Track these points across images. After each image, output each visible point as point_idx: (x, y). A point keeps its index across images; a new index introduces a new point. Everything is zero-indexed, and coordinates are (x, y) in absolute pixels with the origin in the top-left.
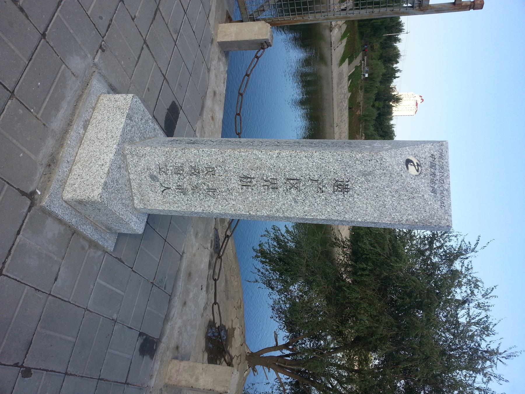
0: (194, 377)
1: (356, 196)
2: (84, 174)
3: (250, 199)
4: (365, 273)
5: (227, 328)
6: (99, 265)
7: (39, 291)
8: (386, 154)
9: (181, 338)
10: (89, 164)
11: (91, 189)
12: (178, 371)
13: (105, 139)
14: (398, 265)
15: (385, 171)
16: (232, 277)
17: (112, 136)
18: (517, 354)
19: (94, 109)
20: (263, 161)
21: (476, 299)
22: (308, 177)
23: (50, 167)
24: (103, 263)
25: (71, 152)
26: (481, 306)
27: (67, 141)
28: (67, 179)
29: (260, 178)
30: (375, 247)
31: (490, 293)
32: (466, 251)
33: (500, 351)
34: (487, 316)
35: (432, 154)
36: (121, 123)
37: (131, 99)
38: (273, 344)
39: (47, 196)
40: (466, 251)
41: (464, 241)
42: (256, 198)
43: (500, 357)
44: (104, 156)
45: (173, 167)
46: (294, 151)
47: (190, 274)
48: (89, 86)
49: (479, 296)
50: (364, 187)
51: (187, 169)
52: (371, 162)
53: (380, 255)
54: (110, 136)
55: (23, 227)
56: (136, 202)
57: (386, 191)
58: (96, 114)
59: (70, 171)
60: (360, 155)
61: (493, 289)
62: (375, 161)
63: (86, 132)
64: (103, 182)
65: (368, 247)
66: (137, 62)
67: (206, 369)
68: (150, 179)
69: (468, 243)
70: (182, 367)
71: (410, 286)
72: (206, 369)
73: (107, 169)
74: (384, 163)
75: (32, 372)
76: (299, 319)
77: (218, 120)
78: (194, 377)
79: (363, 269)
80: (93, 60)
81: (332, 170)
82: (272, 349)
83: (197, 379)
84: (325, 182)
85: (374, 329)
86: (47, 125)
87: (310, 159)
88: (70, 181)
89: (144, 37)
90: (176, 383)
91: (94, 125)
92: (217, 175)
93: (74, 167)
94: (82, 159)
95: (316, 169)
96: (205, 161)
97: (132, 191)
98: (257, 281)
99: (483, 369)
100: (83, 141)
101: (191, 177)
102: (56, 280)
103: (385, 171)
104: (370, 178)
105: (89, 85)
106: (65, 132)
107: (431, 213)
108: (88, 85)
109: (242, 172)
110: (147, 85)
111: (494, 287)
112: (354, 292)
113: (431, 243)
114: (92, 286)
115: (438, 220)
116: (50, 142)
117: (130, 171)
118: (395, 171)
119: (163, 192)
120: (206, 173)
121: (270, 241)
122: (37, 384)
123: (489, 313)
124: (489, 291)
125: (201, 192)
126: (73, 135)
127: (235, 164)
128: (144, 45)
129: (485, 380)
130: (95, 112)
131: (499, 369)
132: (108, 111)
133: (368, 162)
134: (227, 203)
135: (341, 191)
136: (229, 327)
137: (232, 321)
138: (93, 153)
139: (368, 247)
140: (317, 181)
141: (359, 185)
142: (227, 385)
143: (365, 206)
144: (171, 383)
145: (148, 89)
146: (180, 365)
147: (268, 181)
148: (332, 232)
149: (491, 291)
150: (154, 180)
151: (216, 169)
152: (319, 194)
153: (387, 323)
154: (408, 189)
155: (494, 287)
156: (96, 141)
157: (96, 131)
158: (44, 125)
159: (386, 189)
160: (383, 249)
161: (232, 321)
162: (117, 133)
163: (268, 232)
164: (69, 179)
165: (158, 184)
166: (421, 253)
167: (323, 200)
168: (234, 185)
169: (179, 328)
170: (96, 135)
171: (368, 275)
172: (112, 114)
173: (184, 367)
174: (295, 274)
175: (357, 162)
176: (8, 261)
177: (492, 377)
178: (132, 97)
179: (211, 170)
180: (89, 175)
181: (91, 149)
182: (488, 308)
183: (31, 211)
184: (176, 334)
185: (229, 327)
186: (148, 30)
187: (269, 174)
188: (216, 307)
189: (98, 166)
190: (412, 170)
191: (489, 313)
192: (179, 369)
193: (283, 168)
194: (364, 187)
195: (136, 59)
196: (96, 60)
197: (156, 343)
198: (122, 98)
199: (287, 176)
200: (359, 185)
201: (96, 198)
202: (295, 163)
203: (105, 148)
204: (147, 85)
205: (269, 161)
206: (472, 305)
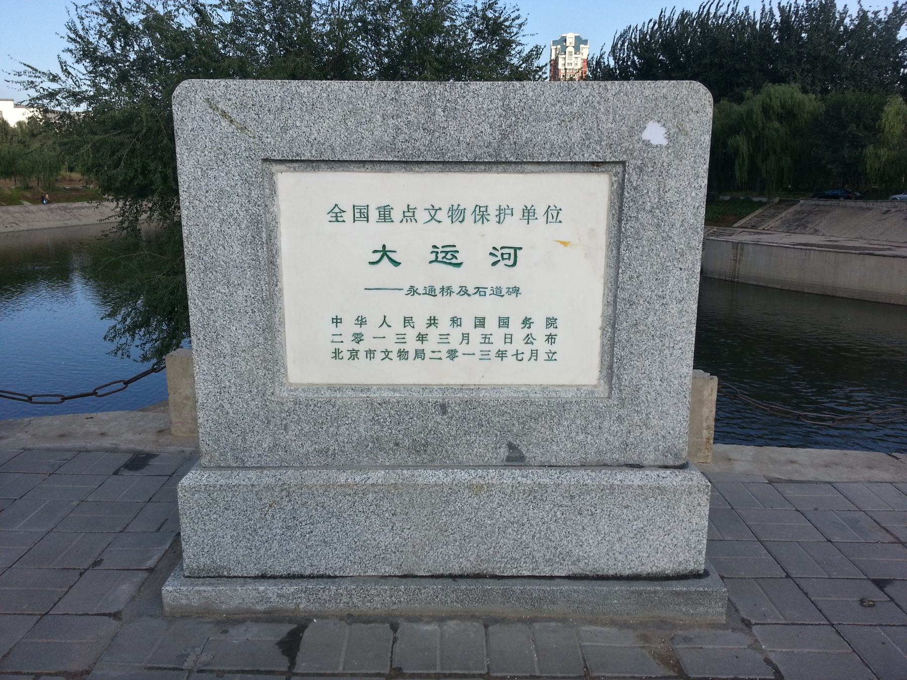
0: (185, 402)
4: (172, 174)
14: (144, 120)
30: (120, 159)
41: (87, 6)
47: (62, 436)
78: (185, 402)
113: (104, 60)
121: (137, 342)
146: (176, 423)
148: (112, 235)
160: (122, 144)
163: (118, 349)
166: (123, 77)
188: (100, 392)
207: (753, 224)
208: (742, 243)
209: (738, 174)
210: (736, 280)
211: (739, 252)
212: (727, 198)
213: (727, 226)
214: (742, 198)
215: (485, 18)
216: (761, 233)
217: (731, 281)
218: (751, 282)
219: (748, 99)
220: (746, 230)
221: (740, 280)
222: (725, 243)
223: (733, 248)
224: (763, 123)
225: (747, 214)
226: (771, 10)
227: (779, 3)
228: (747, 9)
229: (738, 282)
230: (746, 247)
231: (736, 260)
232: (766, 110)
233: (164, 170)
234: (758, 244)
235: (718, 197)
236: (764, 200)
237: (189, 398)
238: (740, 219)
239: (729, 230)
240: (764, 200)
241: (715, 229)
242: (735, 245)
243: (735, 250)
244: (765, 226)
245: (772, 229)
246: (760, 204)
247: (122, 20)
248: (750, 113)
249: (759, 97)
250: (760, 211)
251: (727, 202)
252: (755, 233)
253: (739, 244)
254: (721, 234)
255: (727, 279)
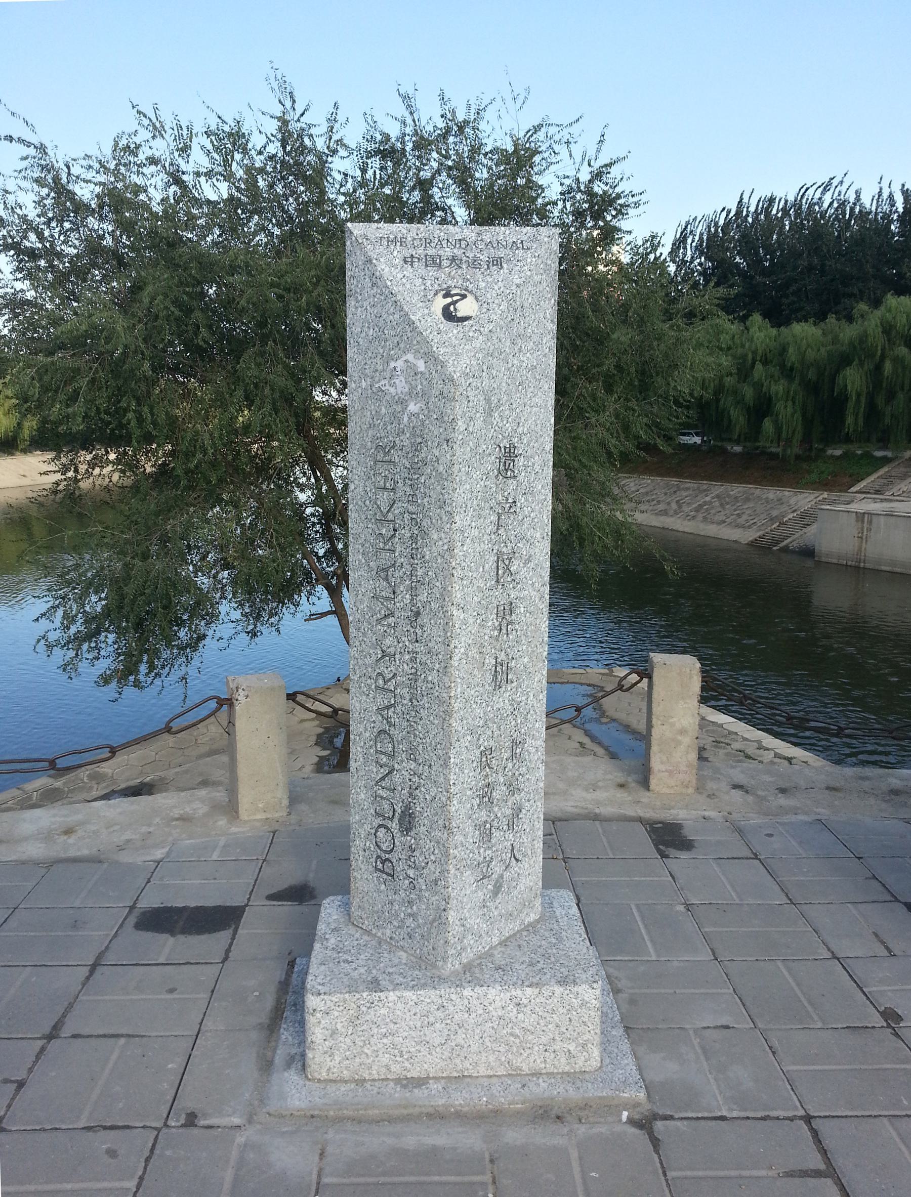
0: (679, 738)
1: (520, 430)
2: (544, 1040)
3: (526, 660)
5: (321, 730)
6: (630, 964)
7: (771, 1048)
8: (453, 365)
9: (600, 784)
10: (517, 1036)
11: (579, 1011)
12: (670, 773)
13: (448, 1021)
15: (485, 368)
16: (199, 741)
17: (438, 1009)
18: (279, 77)
19: (361, 1082)
20: (470, 642)
21: (168, 154)
22: (493, 536)
23: (560, 1115)
24: (619, 958)
25: (499, 1089)
26: (182, 144)
27: (481, 1105)
28: (558, 1073)
29: (495, 643)
31: (150, 120)
32: (45, 168)
33: (278, 111)
34: (208, 134)
35: (402, 262)
36: (402, 999)
37: (326, 997)
38: (333, 620)
39: (625, 1095)
40: (45, 168)
42: (524, 647)
43: (291, 116)
44: (495, 1009)
45: (479, 847)
46: (454, 572)
48: (316, 1113)
49: (159, 143)
50: (507, 412)
51: (483, 815)
52: (471, 398)
53: (93, 380)
54: (440, 1014)
55: (706, 1115)
56: (533, 917)
57: (513, 366)
58: (374, 1072)
59: (537, 1074)
60: (460, 423)
61: (139, 112)
62: (469, 389)
63: (428, 1078)
64: (562, 989)
65: (78, 408)
66: (129, 1036)
67: (661, 718)
68: (500, 895)
69: (25, 164)
70: (663, 768)
71: (166, 308)
72: (661, 718)
73: (529, 991)
74: (473, 370)
75: (883, 1008)
76: (278, 566)
77: (58, 819)
78: (679, 738)
79: (140, 420)
80: (243, 1128)
81: (482, 483)
82: (343, 622)
83: (683, 732)
84: (500, 498)
85: (277, 395)
86: (487, 1156)
87: (466, 535)
88: (563, 1065)
89: (40, 1043)
90: (694, 771)
91: (407, 1064)
92: (492, 743)
93: (526, 1069)
94: (503, 1059)
95: (482, 520)
96: (471, 775)
97: (518, 931)
98: (184, 678)
99: (319, 156)
100: (455, 1074)
101: (495, 801)
102: (727, 1027)
103: (485, 368)
104: (494, 399)
105: (312, 1112)
106: (461, 1117)
107: (542, 271)
108: (313, 1116)
109: (487, 687)
110: (163, 997)
111: (135, 110)
112: (197, 441)
113: (33, 254)
114: (676, 964)
115: (552, 256)
116: (513, 1136)
117: (488, 947)
118: (484, 346)
119: (517, 860)
120: (490, 768)
122: (889, 994)
123: (199, 128)
124: (146, 122)
125: (517, 773)
126: (459, 1099)
127: (474, 706)
128: (63, 1035)
129: (342, 152)
130: (370, 1074)
131: (317, 120)
132: (365, 1045)
133: (471, 404)
134: (532, 712)
135: (514, 461)
136: (317, 726)
137: (302, 721)
138: (487, 1040)
139: (78, 408)
140: (499, 515)
141: (505, 422)
142: (688, 670)
143: (534, 409)
144: (694, 781)
145: (171, 991)
146: (659, 771)
147: (500, 625)
149: (145, 116)
150: (501, 886)
151: (482, 748)
152: (518, 510)
153: (258, 365)
154: (509, 319)
155: (135, 110)
156: (453, 1044)
157: (426, 1053)
158: (492, 1161)
159: (510, 365)
161: (302, 721)
162: (429, 1001)
164: (556, 1071)
165: (507, 875)
167: (526, 500)
168: (506, 701)
169: (586, 789)
170: (438, 1050)
171: (151, 409)
172: (375, 1030)
173: (662, 763)
174: (174, 586)
175: (470, 429)
176: (781, 1114)
177: (335, 138)
178: (322, 997)
179: (484, 759)
180: (544, 1028)
181: (475, 1048)
182: (185, 129)
183: (668, 1113)
184: (601, 795)
185: (317, 726)
186: (8, 1041)
187: (490, 624)
188: (175, 725)
189: (521, 1016)
190: (465, 308)
191: (199, 128)
192: (666, 771)
193: (481, 595)
194: (507, 412)
195: (122, 1041)
196: (236, 1121)
197: (651, 825)
198: (323, 1022)
199: (493, 582)
200: (505, 422)
201: (598, 992)
202: (473, 568)
203: (473, 1015)
204: (163, 997)
205: (470, 628)
206: (183, 167)
207: (878, 488)
208: (870, 514)
209: (850, 420)
210: (862, 565)
211: (865, 525)
212: (838, 452)
213: (840, 491)
214: (859, 452)
215: (590, 193)
216: (891, 501)
217: (855, 567)
218: (884, 568)
219: (862, 316)
220: (869, 496)
221: (867, 565)
222: (845, 514)
223: (857, 521)
224: (883, 350)
225: (869, 475)
226: (891, 197)
227: (903, 185)
228: (858, 193)
229: (864, 568)
230: (875, 519)
231: (861, 538)
232: (888, 329)
233: (138, 408)
234: (892, 515)
235: (825, 452)
236: (889, 454)
237: (686, 731)
238: (859, 481)
239: (845, 496)
240: (889, 454)
241: (825, 495)
242: (860, 517)
243: (860, 523)
244: (894, 490)
245: (905, 494)
246: (886, 461)
247: (71, 195)
248: (863, 338)
249: (878, 313)
250: (885, 469)
251: (838, 458)
252: (882, 500)
253: (866, 516)
254: (834, 502)
255: (850, 563)
